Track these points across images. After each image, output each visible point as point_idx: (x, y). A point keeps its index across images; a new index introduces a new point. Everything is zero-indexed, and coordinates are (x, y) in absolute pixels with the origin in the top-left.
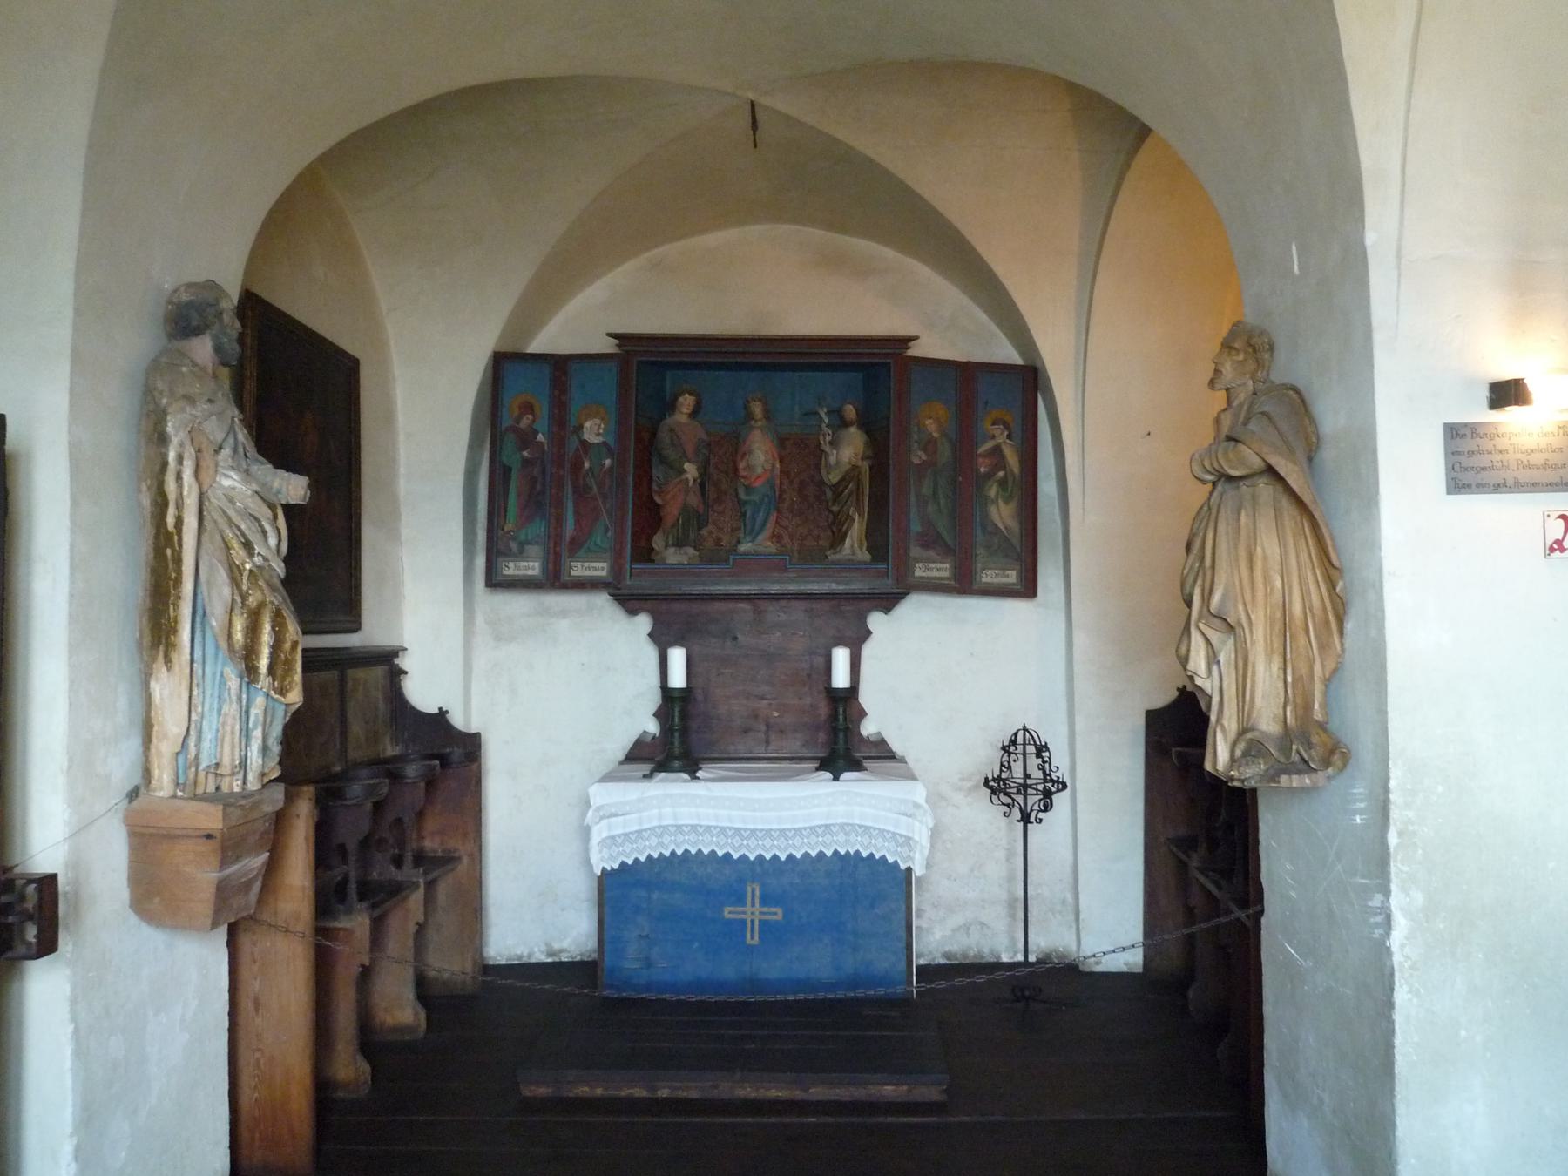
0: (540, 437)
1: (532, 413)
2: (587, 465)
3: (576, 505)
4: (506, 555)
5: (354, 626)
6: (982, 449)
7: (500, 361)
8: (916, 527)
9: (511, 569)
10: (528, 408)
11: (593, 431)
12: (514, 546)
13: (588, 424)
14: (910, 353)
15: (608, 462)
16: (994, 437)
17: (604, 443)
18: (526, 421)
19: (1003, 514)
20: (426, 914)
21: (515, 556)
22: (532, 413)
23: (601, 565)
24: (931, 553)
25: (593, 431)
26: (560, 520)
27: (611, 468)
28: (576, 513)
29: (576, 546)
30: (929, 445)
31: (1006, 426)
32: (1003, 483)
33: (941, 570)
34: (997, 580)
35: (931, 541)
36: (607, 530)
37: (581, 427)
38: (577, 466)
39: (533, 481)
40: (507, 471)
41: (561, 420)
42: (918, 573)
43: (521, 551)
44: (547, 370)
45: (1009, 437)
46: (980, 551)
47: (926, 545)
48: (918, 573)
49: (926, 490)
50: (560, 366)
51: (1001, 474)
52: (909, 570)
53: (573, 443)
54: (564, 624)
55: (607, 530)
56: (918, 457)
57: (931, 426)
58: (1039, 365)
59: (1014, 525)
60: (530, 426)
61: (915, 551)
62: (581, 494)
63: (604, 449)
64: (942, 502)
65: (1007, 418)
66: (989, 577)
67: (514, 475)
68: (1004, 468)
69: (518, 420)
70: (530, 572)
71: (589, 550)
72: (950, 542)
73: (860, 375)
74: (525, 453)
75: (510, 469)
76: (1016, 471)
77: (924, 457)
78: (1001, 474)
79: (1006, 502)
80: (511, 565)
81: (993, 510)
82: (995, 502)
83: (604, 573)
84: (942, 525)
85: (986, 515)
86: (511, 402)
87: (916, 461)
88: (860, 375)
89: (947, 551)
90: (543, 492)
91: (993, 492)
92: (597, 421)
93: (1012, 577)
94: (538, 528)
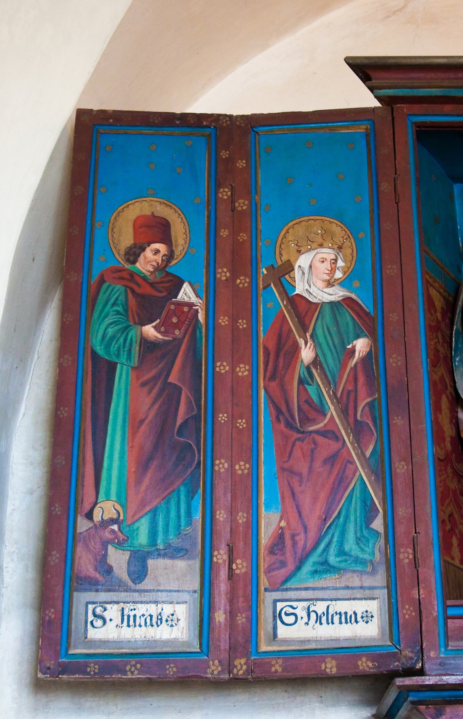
0: (186, 293)
1: (166, 238)
2: (307, 354)
3: (284, 452)
4: (91, 584)
5: (291, 268)
7: (93, 134)
9: (110, 626)
10: (159, 229)
11: (318, 273)
12: (118, 559)
13: (303, 261)
15: (361, 345)
17: (347, 300)
18: (150, 259)
20: (457, 419)
21: (115, 586)
22: (166, 238)
23: (360, 607)
25: (318, 273)
26: (246, 493)
27: (367, 360)
28: (286, 471)
29: (291, 558)
36: (370, 512)
37: (288, 267)
38: (284, 350)
39: (170, 396)
40: (104, 372)
41: (238, 253)
43: (139, 572)
44: (199, 148)
50: (231, 141)
53: (271, 304)
54: (34, 647)
55: (370, 512)
60: (161, 268)
62: (295, 419)
63: (347, 317)
65: (83, 602)
67: (419, 129)
69: (133, 254)
70: (163, 633)
71: (325, 567)
73: (75, 594)
74: (149, 330)
75: (112, 367)
80: (112, 612)
83: (370, 631)
86: (119, 228)
88: (75, 594)
90: (195, 420)
92: (327, 253)
94: (185, 513)
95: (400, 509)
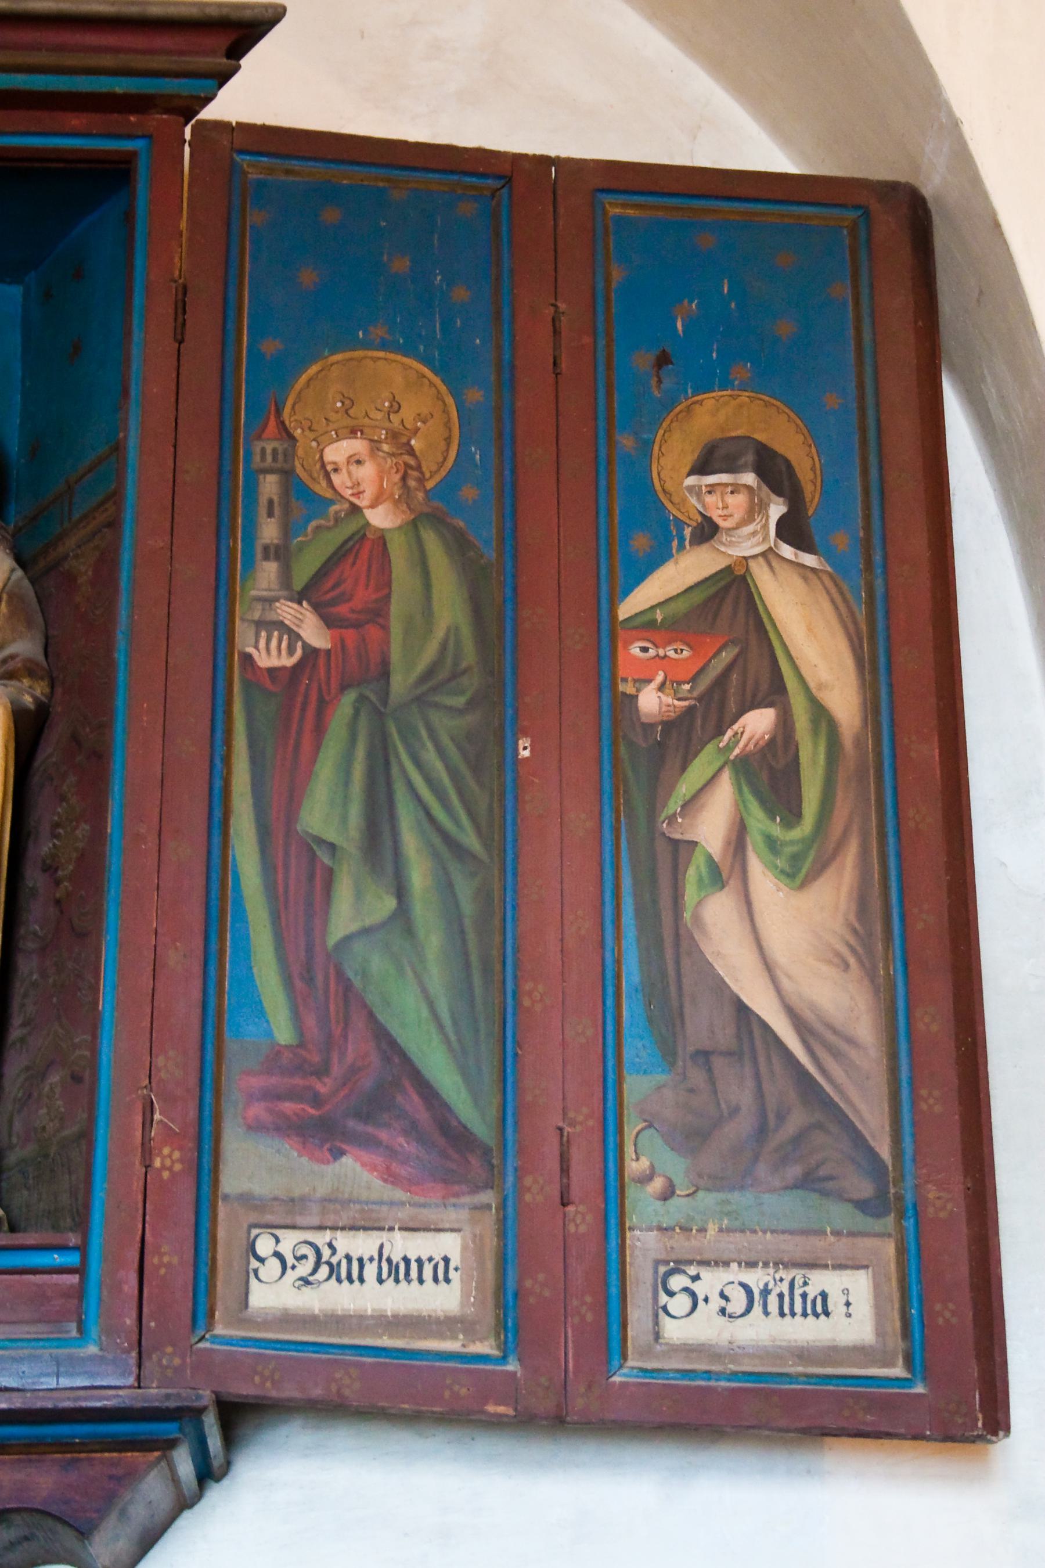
6: (629, 607)
8: (271, 1012)
14: (235, 103)
16: (707, 531)
19: (780, 942)
24: (352, 1172)
30: (348, 577)
31: (774, 472)
32: (771, 777)
33: (412, 1271)
34: (761, 1330)
35: (355, 1098)
42: (272, 1293)
45: (793, 530)
46: (647, 1156)
47: (322, 1133)
48: (272, 1293)
49: (327, 810)
51: (758, 723)
52: (207, 1280)
54: (340, 1313)
56: (282, 631)
57: (354, 469)
58: (934, 182)
59: (843, 1000)
61: (253, 1163)
64: (419, 876)
65: (789, 441)
66: (708, 1315)
68: (774, 693)
72: (481, 1127)
76: (844, 701)
77: (313, 632)
78: (758, 723)
79: (800, 870)
81: (717, 918)
82: (728, 872)
84: (419, 1011)
85: (672, 943)
87: (271, 656)
89: (454, 1157)
91: (710, 828)
93: (849, 1312)
95: (337, 452)
